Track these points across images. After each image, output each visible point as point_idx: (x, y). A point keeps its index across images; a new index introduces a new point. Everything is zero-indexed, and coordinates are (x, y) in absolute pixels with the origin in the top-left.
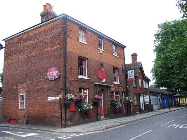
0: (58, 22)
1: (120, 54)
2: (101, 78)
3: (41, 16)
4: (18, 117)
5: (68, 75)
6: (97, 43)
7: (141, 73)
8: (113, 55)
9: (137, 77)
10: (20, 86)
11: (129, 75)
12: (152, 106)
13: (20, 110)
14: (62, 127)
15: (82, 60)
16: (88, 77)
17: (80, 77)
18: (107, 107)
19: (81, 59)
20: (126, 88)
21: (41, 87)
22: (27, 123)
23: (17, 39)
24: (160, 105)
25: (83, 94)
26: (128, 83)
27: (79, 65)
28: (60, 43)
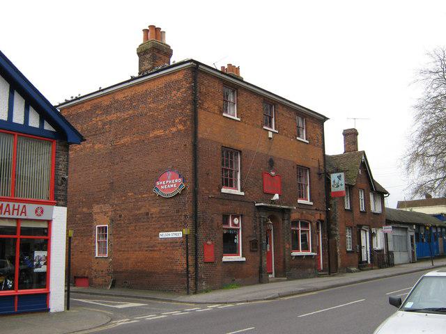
0: (180, 76)
1: (313, 135)
2: (270, 192)
3: (138, 54)
4: (94, 274)
5: (202, 188)
6: (261, 116)
7: (364, 176)
8: (298, 138)
9: (353, 186)
10: (96, 208)
11: (332, 183)
12: (390, 254)
13: (97, 258)
14: (188, 294)
15: (229, 153)
16: (242, 190)
17: (224, 190)
18: (282, 254)
19: (231, 153)
20: (327, 212)
21: (143, 210)
22: (113, 286)
23: (87, 107)
24: (413, 253)
25: (231, 227)
26: (332, 202)
27: (223, 164)
28: (185, 122)
